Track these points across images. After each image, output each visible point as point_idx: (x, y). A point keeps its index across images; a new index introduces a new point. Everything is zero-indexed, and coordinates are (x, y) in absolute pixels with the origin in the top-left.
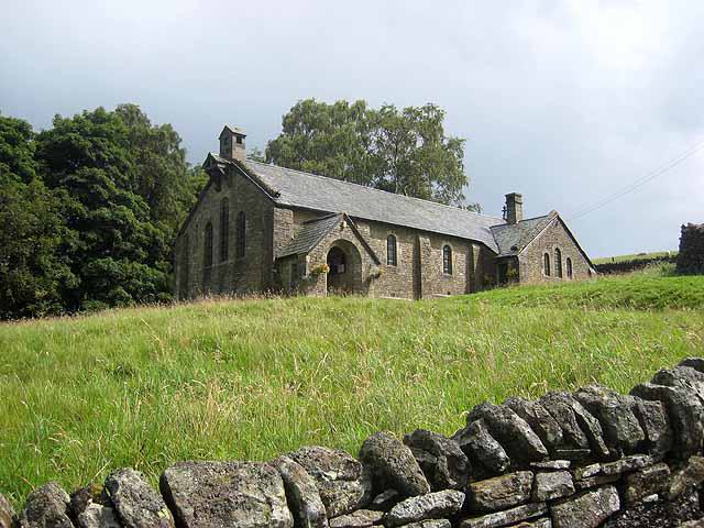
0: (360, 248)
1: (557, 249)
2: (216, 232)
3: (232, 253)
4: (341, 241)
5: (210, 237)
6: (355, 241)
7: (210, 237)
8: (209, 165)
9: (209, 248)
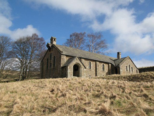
0: (81, 64)
1: (129, 65)
3: (52, 66)
4: (77, 63)
5: (48, 62)
6: (80, 63)
7: (48, 62)
9: (47, 65)
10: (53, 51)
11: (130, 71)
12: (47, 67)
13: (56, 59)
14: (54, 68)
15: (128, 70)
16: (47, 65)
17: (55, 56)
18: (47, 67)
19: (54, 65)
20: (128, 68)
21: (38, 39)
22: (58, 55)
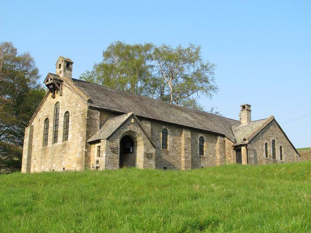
2: (51, 124)
3: (60, 138)
4: (130, 131)
8: (48, 81)
9: (46, 134)
10: (64, 97)
11: (274, 157)
12: (46, 140)
13: (70, 120)
14: (65, 145)
15: (270, 152)
16: (46, 134)
17: (67, 112)
18: (46, 140)
19: (66, 134)
20: (270, 149)
21: (18, 60)
22: (78, 109)
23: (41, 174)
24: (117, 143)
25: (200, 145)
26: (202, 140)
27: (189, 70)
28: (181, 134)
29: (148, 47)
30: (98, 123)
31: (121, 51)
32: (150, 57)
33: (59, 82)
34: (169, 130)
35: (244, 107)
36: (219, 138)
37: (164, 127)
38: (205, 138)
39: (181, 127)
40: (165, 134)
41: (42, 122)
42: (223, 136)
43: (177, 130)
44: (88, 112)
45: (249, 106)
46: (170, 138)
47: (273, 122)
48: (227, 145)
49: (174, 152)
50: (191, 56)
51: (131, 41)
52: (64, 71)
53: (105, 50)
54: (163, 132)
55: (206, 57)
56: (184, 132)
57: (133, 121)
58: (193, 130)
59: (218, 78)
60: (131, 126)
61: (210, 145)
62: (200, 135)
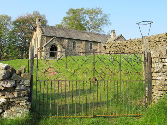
4: (54, 44)
23: (5, 63)
24: (49, 47)
25: (90, 47)
26: (91, 45)
27: (100, 16)
28: (82, 43)
29: (82, 9)
30: (45, 41)
31: (72, 11)
32: (84, 13)
33: (36, 27)
34: (76, 42)
35: (112, 31)
36: (99, 44)
37: (74, 41)
38: (92, 44)
39: (82, 40)
40: (74, 43)
41: (34, 40)
42: (101, 43)
43: (80, 42)
44: (41, 37)
45: (114, 31)
46: (76, 45)
47: (121, 36)
48: (102, 46)
49: (78, 50)
50: (45, 22)
51: (75, 8)
52: (38, 22)
53: (67, 11)
54: (73, 43)
55: (104, 12)
56: (83, 42)
57: (55, 40)
58: (87, 41)
59: (112, 19)
60: (54, 42)
61: (95, 46)
62: (90, 43)
